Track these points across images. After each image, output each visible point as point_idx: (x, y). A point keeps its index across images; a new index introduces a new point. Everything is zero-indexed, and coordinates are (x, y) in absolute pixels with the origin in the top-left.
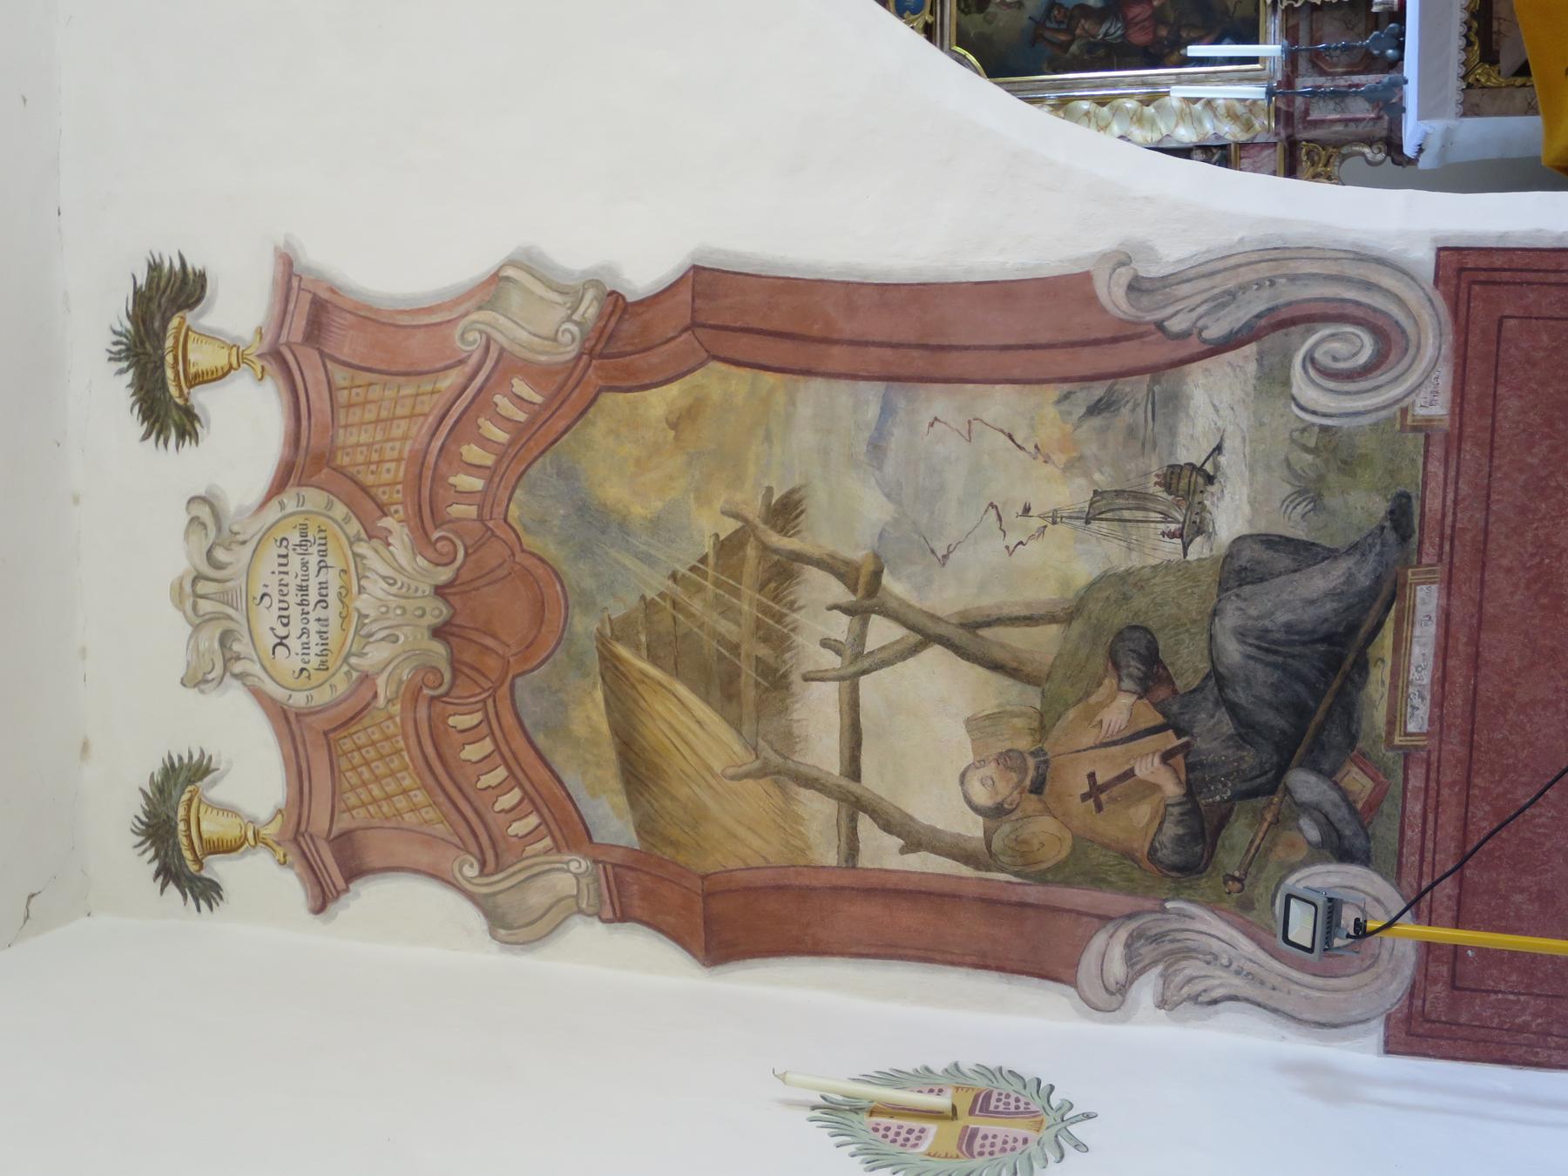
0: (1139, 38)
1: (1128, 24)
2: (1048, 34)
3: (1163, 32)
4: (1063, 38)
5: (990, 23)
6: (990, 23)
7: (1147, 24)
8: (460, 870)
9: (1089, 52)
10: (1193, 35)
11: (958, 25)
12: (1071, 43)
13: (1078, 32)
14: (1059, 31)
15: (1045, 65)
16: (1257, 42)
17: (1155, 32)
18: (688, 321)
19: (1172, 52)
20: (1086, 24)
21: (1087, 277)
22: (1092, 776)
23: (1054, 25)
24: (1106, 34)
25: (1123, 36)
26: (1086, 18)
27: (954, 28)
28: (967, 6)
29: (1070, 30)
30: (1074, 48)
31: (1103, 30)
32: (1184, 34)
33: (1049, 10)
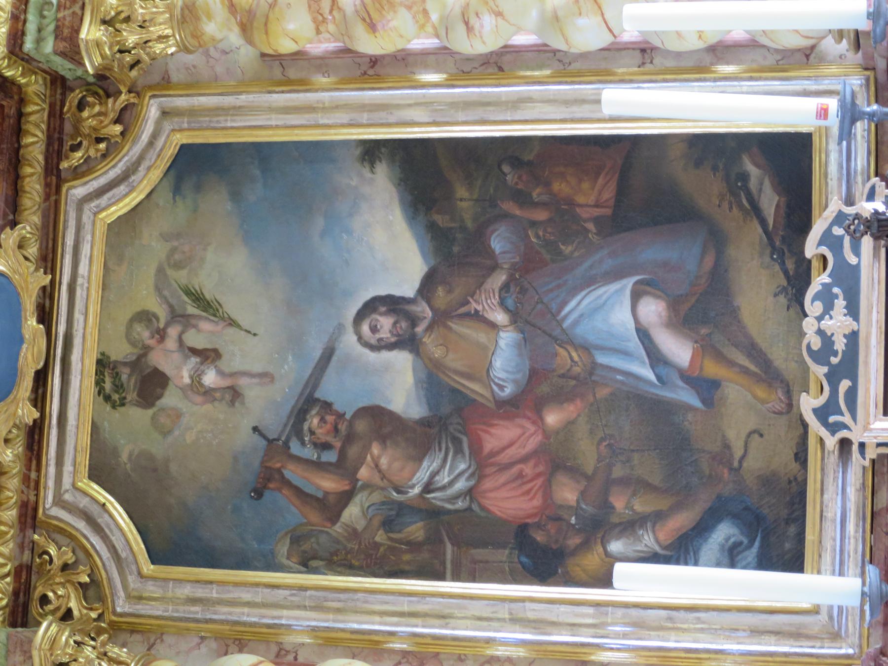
0: (508, 502)
1: (482, 463)
2: (292, 473)
3: (567, 493)
4: (328, 484)
5: (166, 433)
6: (166, 433)
7: (528, 469)
8: (443, 488)
9: (388, 524)
10: (640, 506)
11: (95, 429)
12: (346, 498)
13: (364, 473)
14: (319, 466)
15: (283, 549)
16: (793, 562)
17: (547, 489)
18: (271, 438)
19: (586, 546)
20: (383, 458)
21: (809, 136)
22: (831, 318)
23: (309, 453)
24: (428, 488)
25: (470, 492)
26: (383, 440)
27: (85, 440)
28: (118, 387)
29: (344, 467)
30: (352, 513)
31: (422, 475)
32: (619, 502)
33: (300, 414)
